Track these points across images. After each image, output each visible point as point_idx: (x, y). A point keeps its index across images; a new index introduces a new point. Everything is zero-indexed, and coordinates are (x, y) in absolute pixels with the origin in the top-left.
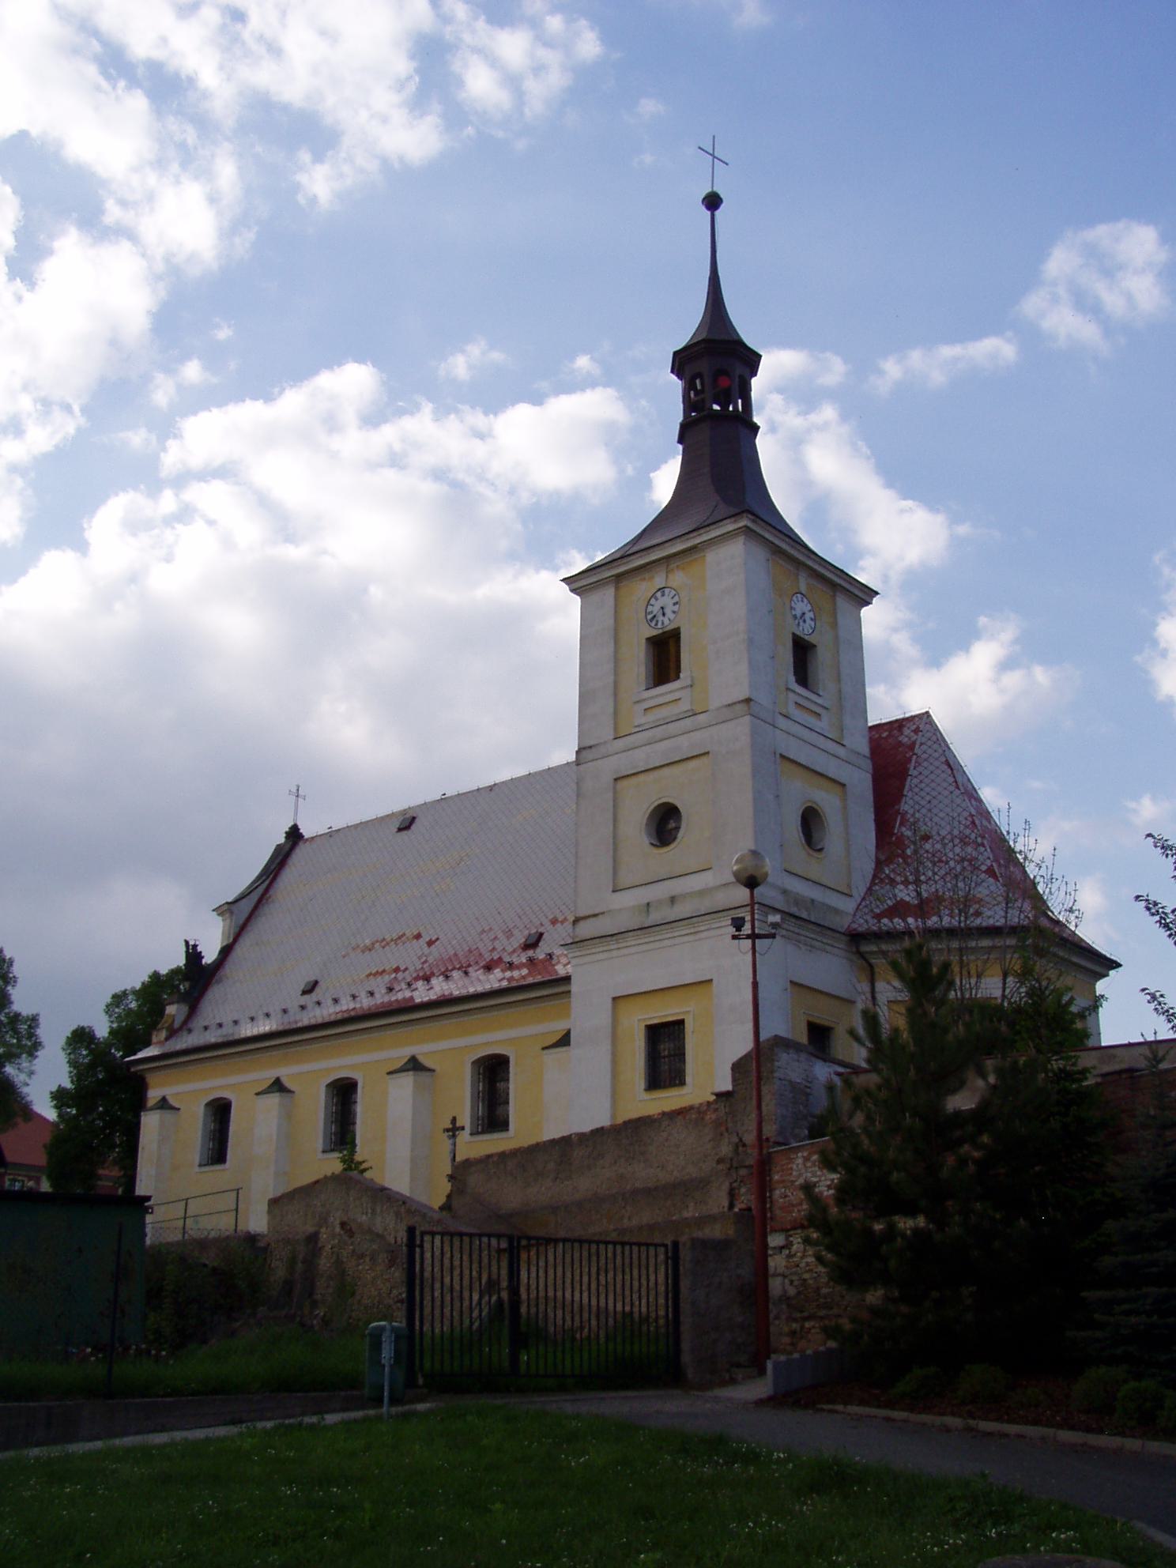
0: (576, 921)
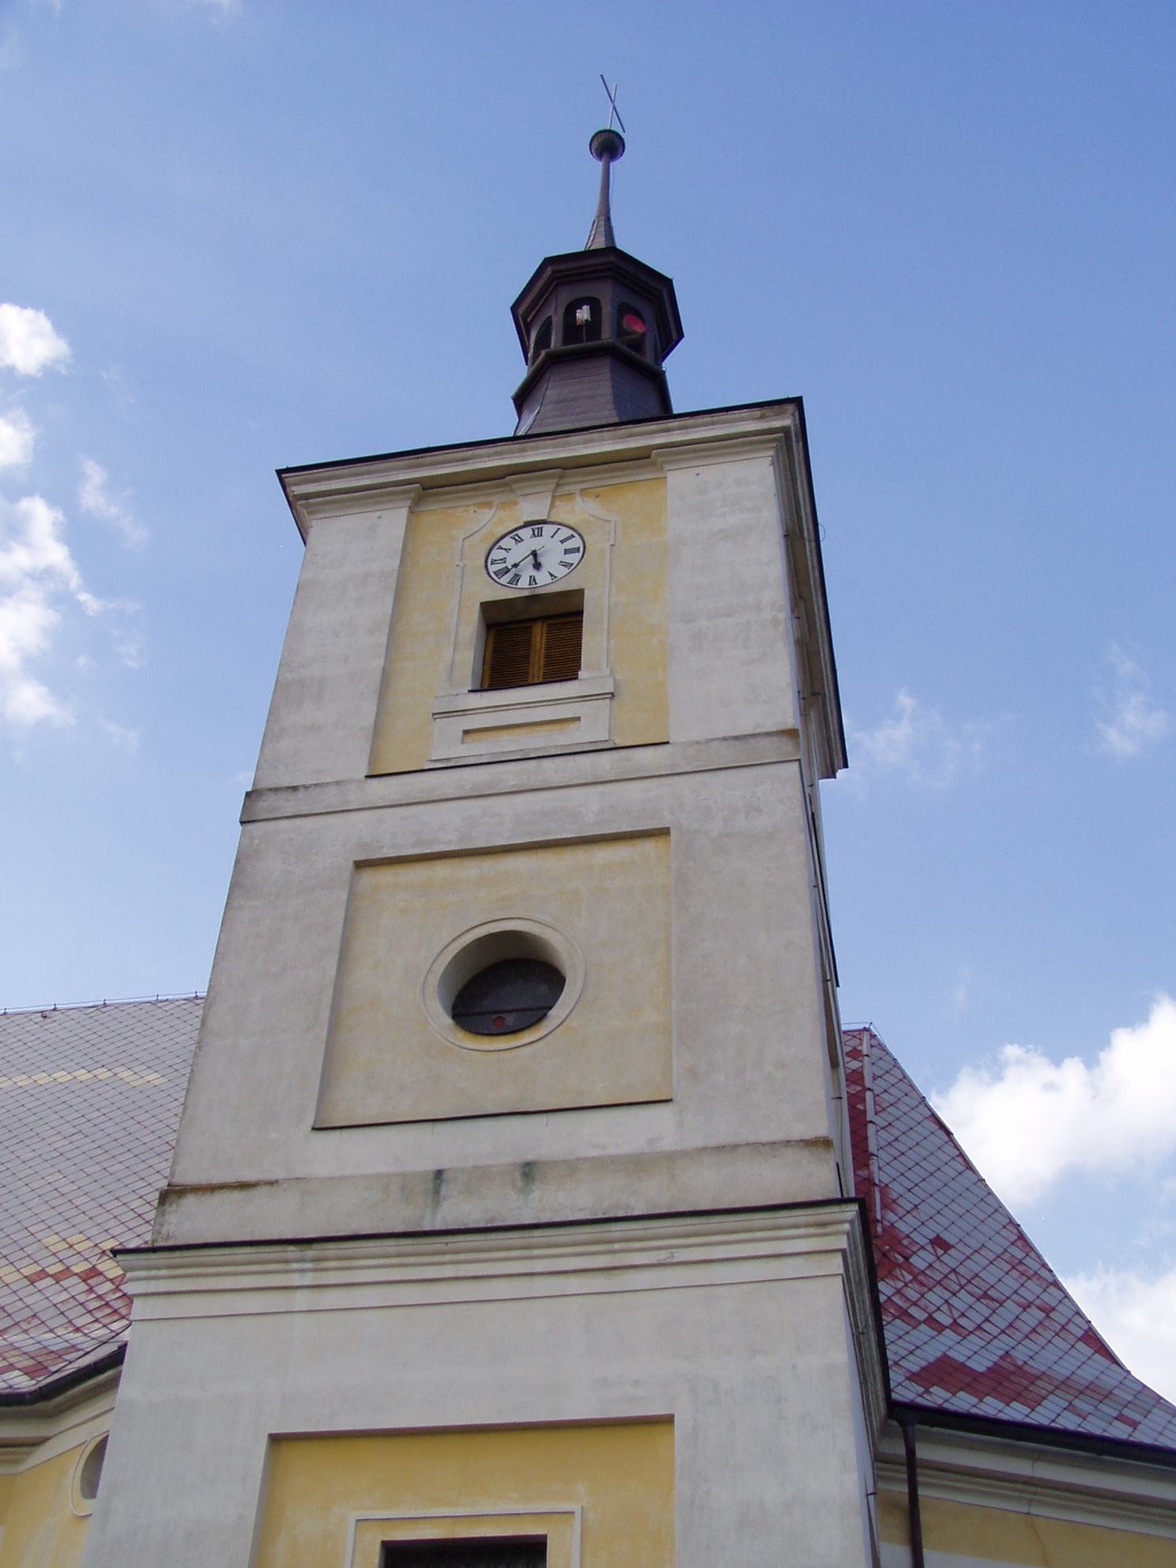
0: (171, 1194)
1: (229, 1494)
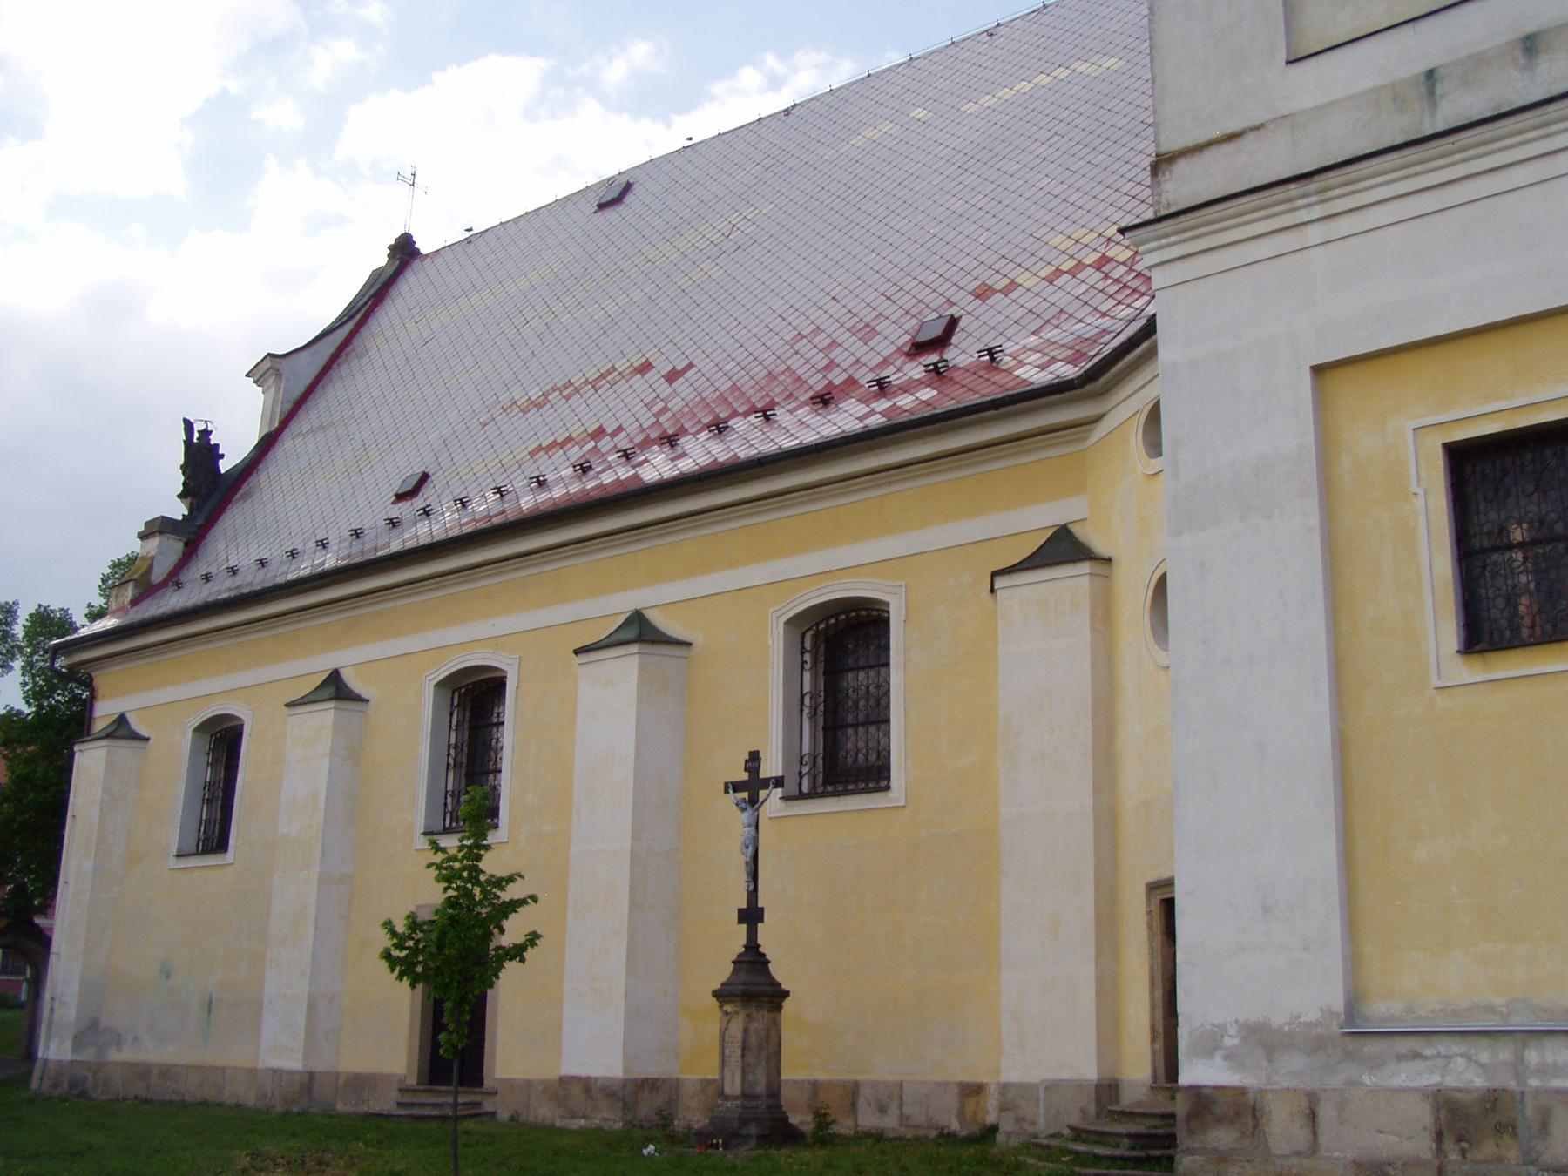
0: (1161, 163)
1: (1288, 425)
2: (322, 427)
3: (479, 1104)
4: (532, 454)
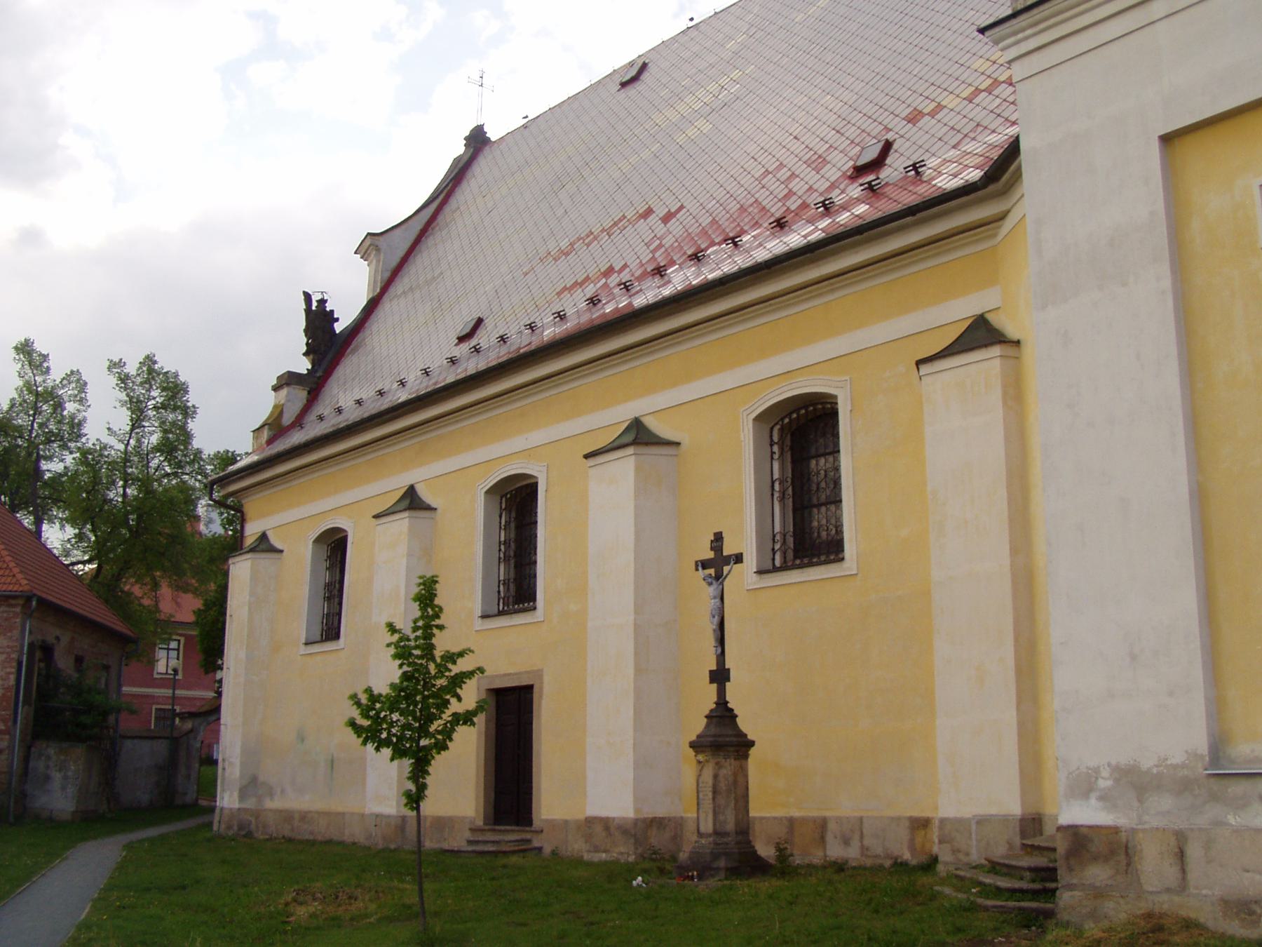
1: (1137, 194)
2: (411, 289)
3: (529, 841)
4: (559, 294)
